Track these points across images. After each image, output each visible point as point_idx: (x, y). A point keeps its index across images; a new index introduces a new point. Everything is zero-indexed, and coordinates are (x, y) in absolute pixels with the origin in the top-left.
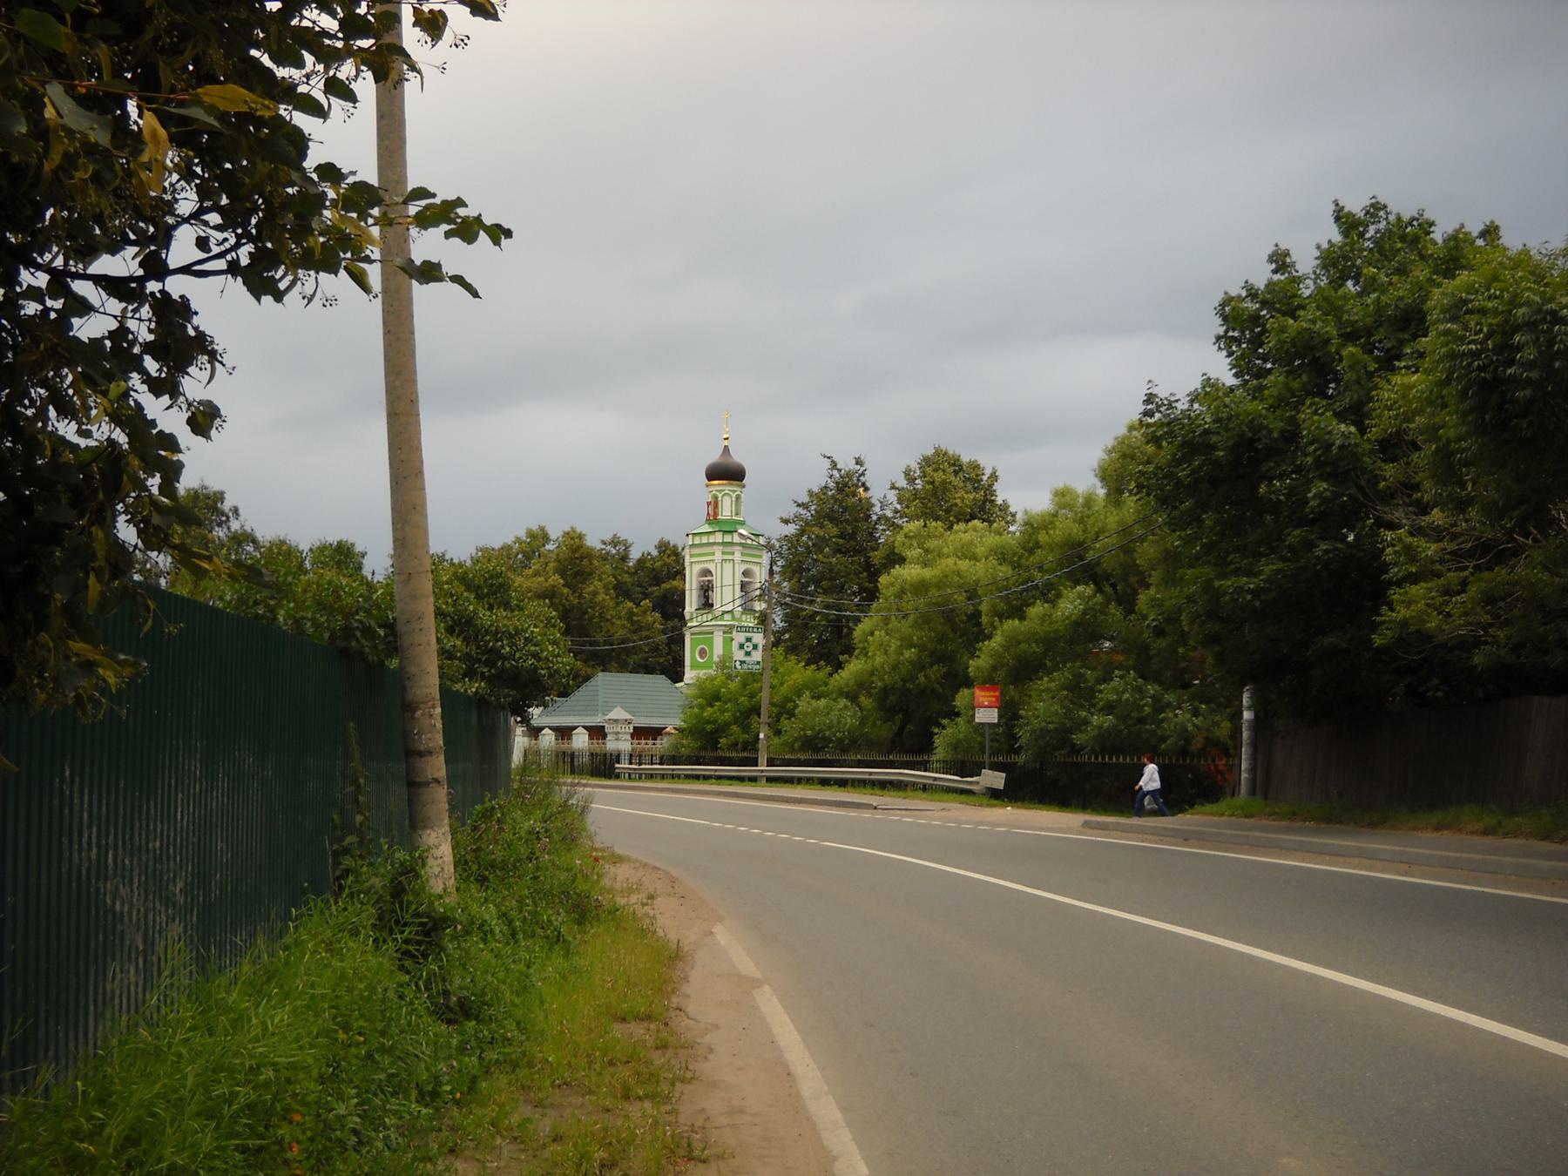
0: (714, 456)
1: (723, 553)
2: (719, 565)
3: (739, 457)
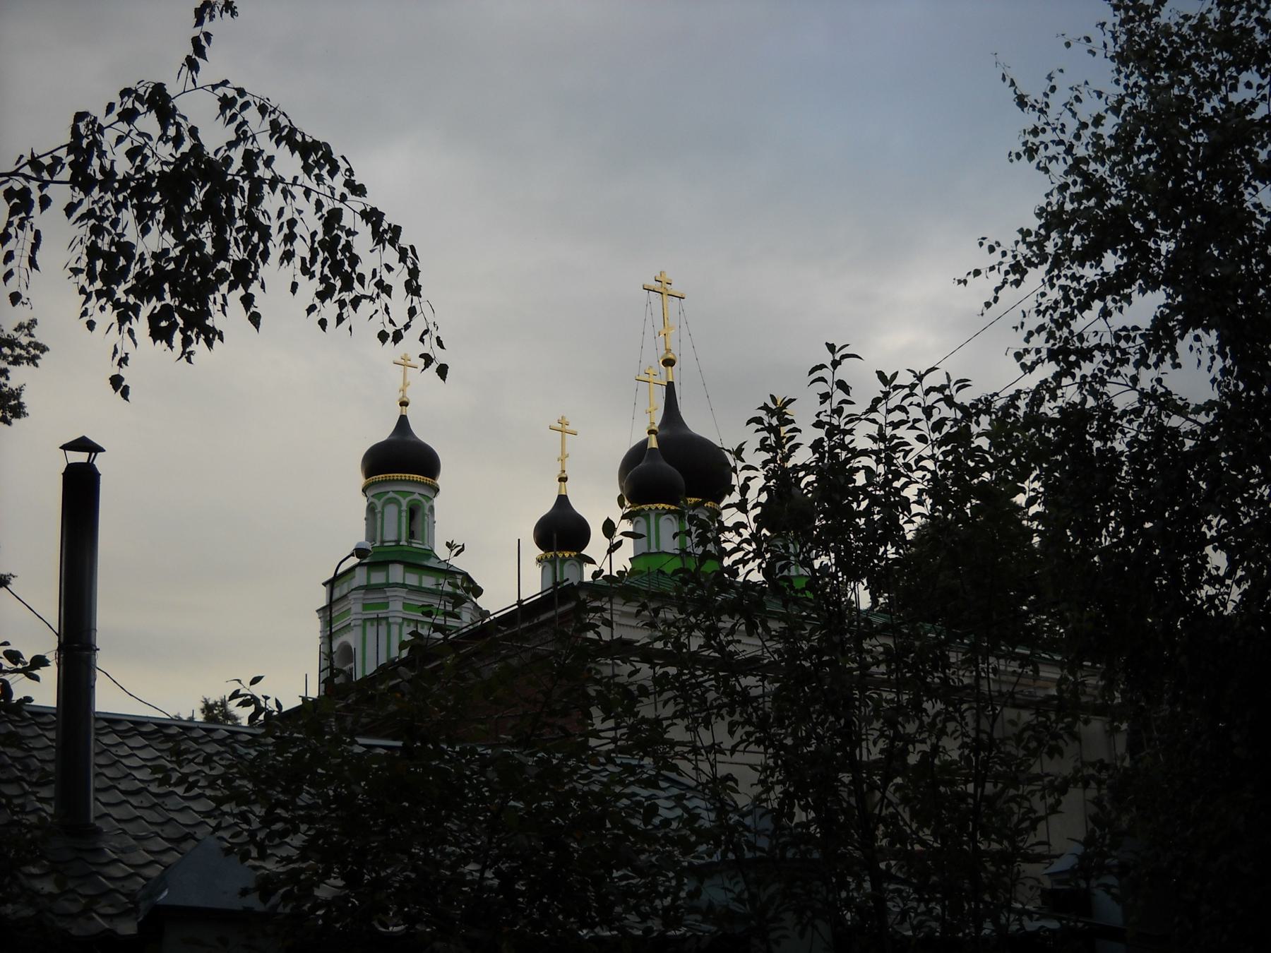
0: (382, 432)
1: (365, 607)
2: (358, 631)
3: (422, 432)
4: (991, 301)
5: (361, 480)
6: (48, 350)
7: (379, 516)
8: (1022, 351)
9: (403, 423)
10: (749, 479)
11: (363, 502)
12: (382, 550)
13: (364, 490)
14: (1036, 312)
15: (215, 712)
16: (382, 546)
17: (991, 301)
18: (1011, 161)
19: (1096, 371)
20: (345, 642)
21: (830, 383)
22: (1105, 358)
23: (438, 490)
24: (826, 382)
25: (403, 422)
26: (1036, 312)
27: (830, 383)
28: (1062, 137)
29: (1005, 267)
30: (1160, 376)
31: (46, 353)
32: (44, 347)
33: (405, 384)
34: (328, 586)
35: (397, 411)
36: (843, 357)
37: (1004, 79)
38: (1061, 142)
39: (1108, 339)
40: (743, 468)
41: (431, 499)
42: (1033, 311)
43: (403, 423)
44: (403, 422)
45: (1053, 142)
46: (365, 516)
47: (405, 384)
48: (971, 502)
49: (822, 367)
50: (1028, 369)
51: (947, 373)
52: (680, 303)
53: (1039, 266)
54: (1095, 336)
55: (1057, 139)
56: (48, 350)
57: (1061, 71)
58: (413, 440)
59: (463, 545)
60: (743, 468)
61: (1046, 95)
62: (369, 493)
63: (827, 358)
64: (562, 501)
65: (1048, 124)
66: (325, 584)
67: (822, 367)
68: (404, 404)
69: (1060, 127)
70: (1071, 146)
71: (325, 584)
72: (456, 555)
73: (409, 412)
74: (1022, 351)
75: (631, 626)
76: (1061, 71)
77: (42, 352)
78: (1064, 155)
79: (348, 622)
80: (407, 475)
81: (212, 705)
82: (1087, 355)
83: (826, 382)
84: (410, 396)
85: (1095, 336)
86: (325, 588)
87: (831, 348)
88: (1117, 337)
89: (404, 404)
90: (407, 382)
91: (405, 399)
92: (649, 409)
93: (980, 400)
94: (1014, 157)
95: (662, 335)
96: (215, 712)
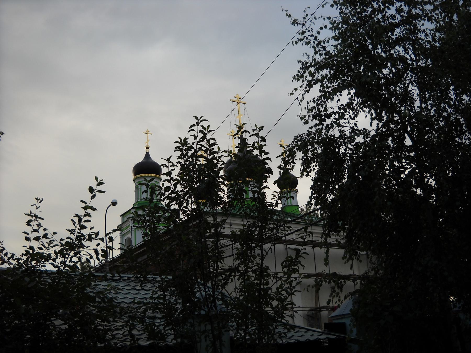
0: (140, 158)
4: (302, 99)
5: (133, 177)
6: (4, 134)
7: (140, 190)
8: (303, 116)
9: (147, 155)
10: (172, 170)
11: (134, 185)
12: (141, 202)
13: (134, 181)
14: (313, 101)
15: (85, 265)
16: (141, 201)
17: (302, 99)
18: (293, 45)
19: (332, 122)
20: (128, 237)
21: (196, 131)
22: (335, 117)
23: (161, 179)
24: (195, 131)
25: (147, 154)
26: (313, 101)
27: (196, 131)
28: (312, 33)
29: (305, 85)
30: (356, 123)
31: (3, 135)
32: (2, 133)
33: (148, 141)
34: (122, 216)
35: (145, 151)
36: (201, 121)
37: (305, 11)
38: (312, 35)
39: (336, 110)
40: (171, 166)
41: (159, 183)
42: (312, 101)
43: (147, 155)
44: (147, 154)
45: (309, 36)
46: (134, 190)
47: (148, 141)
48: (406, 175)
49: (194, 125)
50: (306, 122)
51: (255, 125)
52: (245, 106)
53: (316, 84)
54: (331, 109)
55: (310, 34)
56: (4, 134)
57: (309, 8)
58: (151, 161)
59: (42, 199)
60: (171, 166)
61: (304, 18)
62: (136, 181)
63: (195, 121)
65: (306, 29)
66: (121, 216)
67: (194, 125)
68: (147, 148)
69: (311, 30)
70: (316, 37)
71: (121, 216)
72: (40, 202)
73: (150, 151)
74: (303, 116)
75: (228, 227)
76: (309, 8)
77: (2, 135)
78: (314, 40)
79: (129, 230)
80: (149, 174)
81: (83, 262)
82: (329, 116)
83: (195, 131)
84: (149, 145)
85: (331, 109)
86: (121, 217)
87: (196, 118)
88: (340, 109)
89: (147, 148)
90: (149, 139)
91: (148, 146)
92: (233, 146)
93: (297, 136)
94: (294, 43)
95: (238, 118)
96: (85, 265)
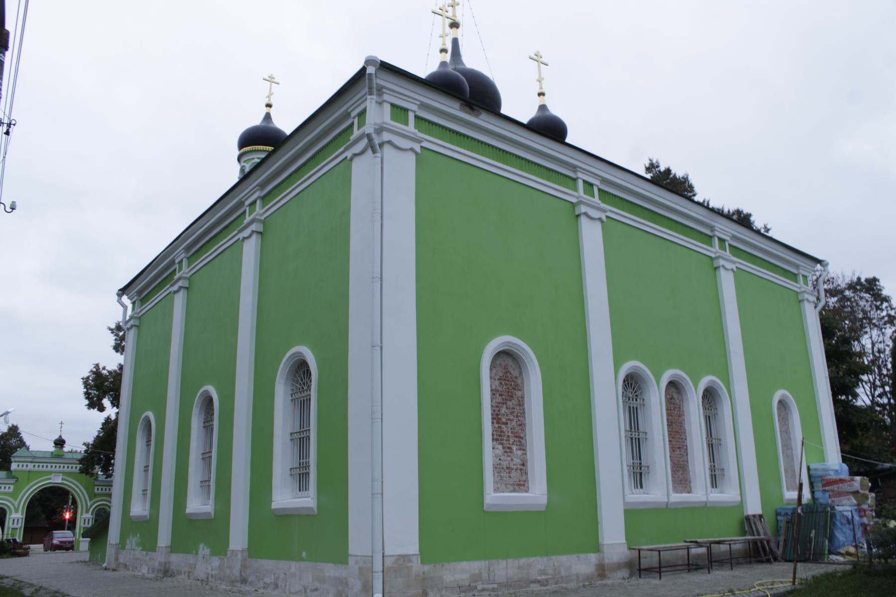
3: (556, 110)
25: (268, 117)
35: (266, 110)
44: (268, 117)
64: (543, 108)
73: (272, 111)
84: (272, 102)
